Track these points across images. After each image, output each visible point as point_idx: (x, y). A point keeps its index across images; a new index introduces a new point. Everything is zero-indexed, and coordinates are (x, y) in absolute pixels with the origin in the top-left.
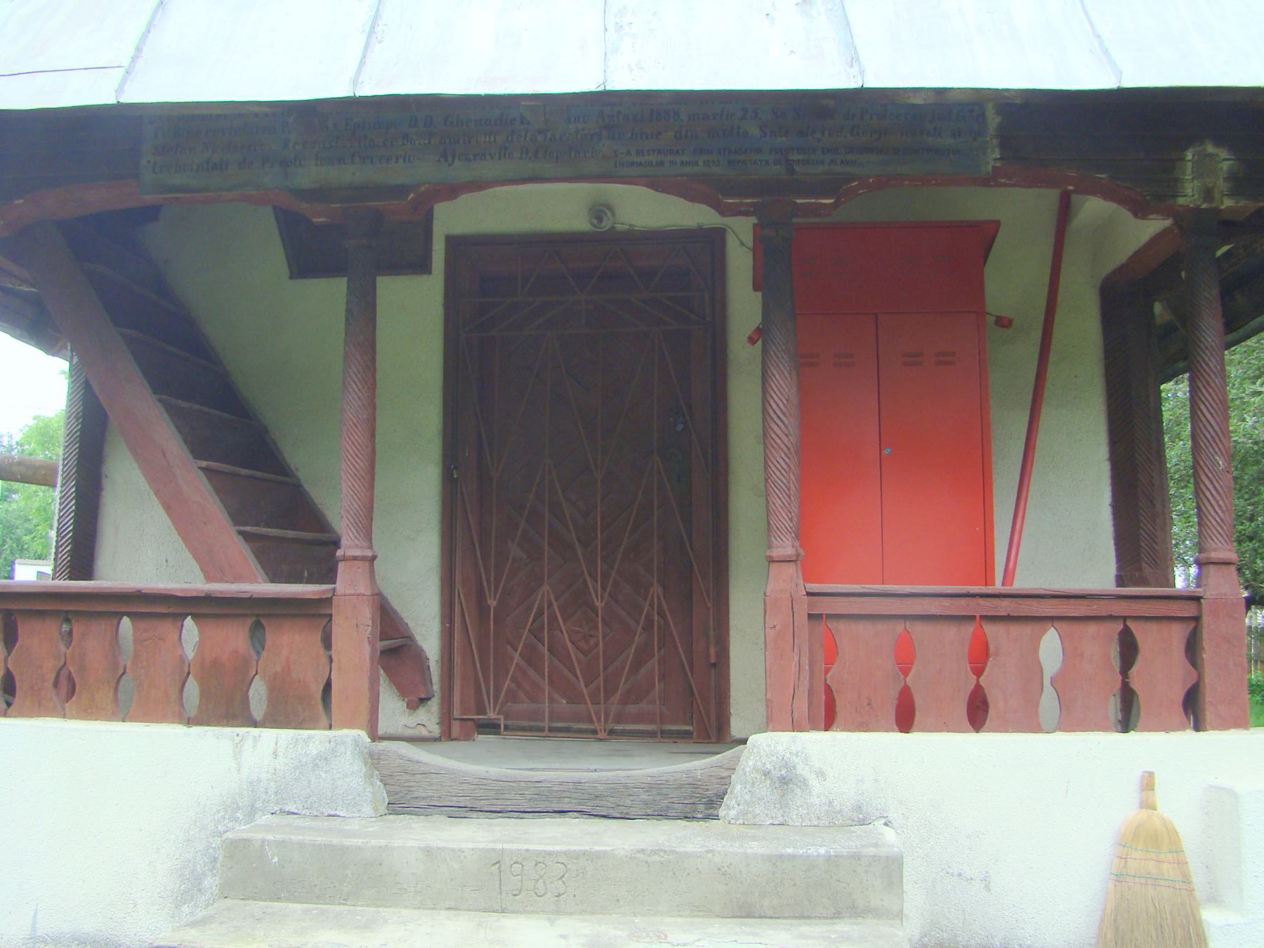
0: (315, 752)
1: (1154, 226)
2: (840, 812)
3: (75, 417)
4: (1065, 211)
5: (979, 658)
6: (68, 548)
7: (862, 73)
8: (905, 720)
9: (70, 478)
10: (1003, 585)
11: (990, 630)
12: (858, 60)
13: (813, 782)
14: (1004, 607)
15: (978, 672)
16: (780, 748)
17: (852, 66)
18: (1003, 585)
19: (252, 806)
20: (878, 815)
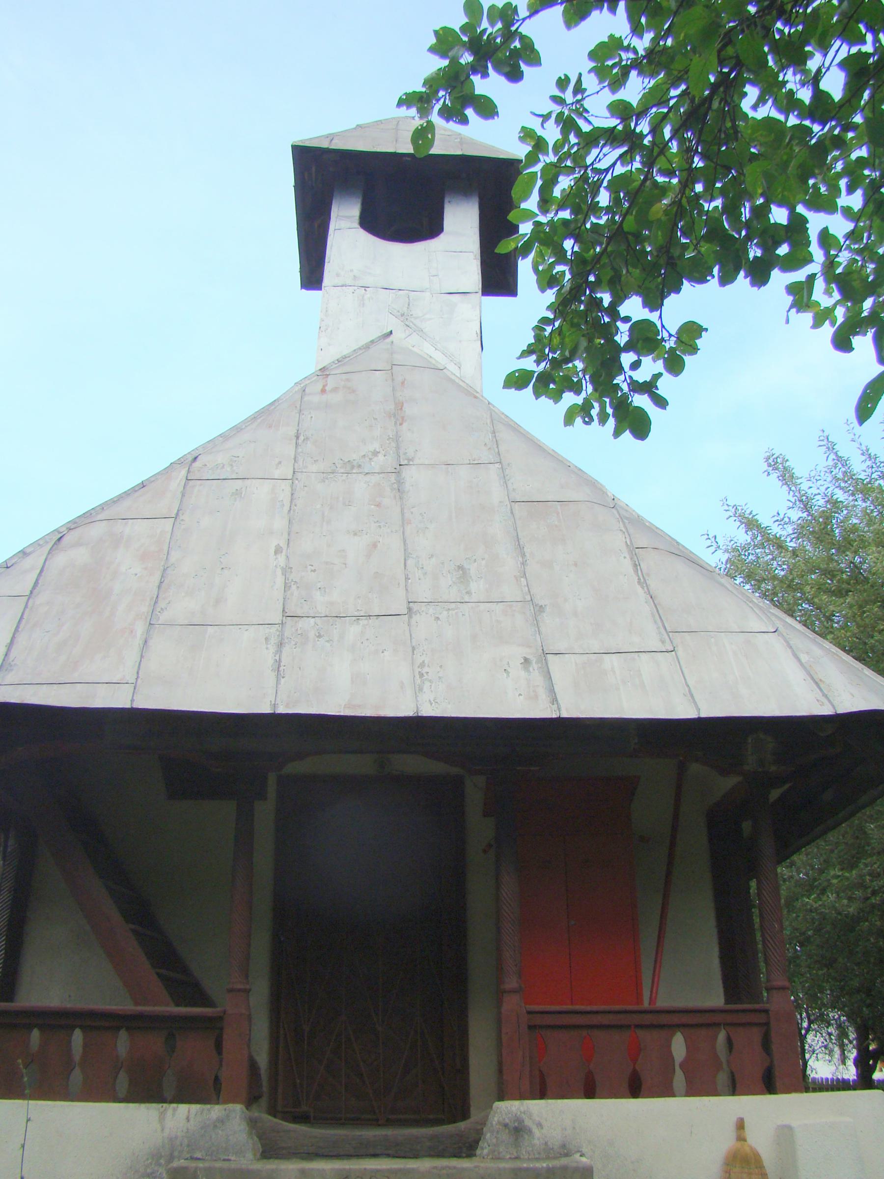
3: (7, 890)
5: (635, 1051)
7: (559, 709)
8: (590, 1092)
11: (640, 1033)
13: (536, 1130)
14: (648, 1019)
15: (634, 1060)
16: (514, 1109)
18: (650, 1004)
20: (576, 1150)
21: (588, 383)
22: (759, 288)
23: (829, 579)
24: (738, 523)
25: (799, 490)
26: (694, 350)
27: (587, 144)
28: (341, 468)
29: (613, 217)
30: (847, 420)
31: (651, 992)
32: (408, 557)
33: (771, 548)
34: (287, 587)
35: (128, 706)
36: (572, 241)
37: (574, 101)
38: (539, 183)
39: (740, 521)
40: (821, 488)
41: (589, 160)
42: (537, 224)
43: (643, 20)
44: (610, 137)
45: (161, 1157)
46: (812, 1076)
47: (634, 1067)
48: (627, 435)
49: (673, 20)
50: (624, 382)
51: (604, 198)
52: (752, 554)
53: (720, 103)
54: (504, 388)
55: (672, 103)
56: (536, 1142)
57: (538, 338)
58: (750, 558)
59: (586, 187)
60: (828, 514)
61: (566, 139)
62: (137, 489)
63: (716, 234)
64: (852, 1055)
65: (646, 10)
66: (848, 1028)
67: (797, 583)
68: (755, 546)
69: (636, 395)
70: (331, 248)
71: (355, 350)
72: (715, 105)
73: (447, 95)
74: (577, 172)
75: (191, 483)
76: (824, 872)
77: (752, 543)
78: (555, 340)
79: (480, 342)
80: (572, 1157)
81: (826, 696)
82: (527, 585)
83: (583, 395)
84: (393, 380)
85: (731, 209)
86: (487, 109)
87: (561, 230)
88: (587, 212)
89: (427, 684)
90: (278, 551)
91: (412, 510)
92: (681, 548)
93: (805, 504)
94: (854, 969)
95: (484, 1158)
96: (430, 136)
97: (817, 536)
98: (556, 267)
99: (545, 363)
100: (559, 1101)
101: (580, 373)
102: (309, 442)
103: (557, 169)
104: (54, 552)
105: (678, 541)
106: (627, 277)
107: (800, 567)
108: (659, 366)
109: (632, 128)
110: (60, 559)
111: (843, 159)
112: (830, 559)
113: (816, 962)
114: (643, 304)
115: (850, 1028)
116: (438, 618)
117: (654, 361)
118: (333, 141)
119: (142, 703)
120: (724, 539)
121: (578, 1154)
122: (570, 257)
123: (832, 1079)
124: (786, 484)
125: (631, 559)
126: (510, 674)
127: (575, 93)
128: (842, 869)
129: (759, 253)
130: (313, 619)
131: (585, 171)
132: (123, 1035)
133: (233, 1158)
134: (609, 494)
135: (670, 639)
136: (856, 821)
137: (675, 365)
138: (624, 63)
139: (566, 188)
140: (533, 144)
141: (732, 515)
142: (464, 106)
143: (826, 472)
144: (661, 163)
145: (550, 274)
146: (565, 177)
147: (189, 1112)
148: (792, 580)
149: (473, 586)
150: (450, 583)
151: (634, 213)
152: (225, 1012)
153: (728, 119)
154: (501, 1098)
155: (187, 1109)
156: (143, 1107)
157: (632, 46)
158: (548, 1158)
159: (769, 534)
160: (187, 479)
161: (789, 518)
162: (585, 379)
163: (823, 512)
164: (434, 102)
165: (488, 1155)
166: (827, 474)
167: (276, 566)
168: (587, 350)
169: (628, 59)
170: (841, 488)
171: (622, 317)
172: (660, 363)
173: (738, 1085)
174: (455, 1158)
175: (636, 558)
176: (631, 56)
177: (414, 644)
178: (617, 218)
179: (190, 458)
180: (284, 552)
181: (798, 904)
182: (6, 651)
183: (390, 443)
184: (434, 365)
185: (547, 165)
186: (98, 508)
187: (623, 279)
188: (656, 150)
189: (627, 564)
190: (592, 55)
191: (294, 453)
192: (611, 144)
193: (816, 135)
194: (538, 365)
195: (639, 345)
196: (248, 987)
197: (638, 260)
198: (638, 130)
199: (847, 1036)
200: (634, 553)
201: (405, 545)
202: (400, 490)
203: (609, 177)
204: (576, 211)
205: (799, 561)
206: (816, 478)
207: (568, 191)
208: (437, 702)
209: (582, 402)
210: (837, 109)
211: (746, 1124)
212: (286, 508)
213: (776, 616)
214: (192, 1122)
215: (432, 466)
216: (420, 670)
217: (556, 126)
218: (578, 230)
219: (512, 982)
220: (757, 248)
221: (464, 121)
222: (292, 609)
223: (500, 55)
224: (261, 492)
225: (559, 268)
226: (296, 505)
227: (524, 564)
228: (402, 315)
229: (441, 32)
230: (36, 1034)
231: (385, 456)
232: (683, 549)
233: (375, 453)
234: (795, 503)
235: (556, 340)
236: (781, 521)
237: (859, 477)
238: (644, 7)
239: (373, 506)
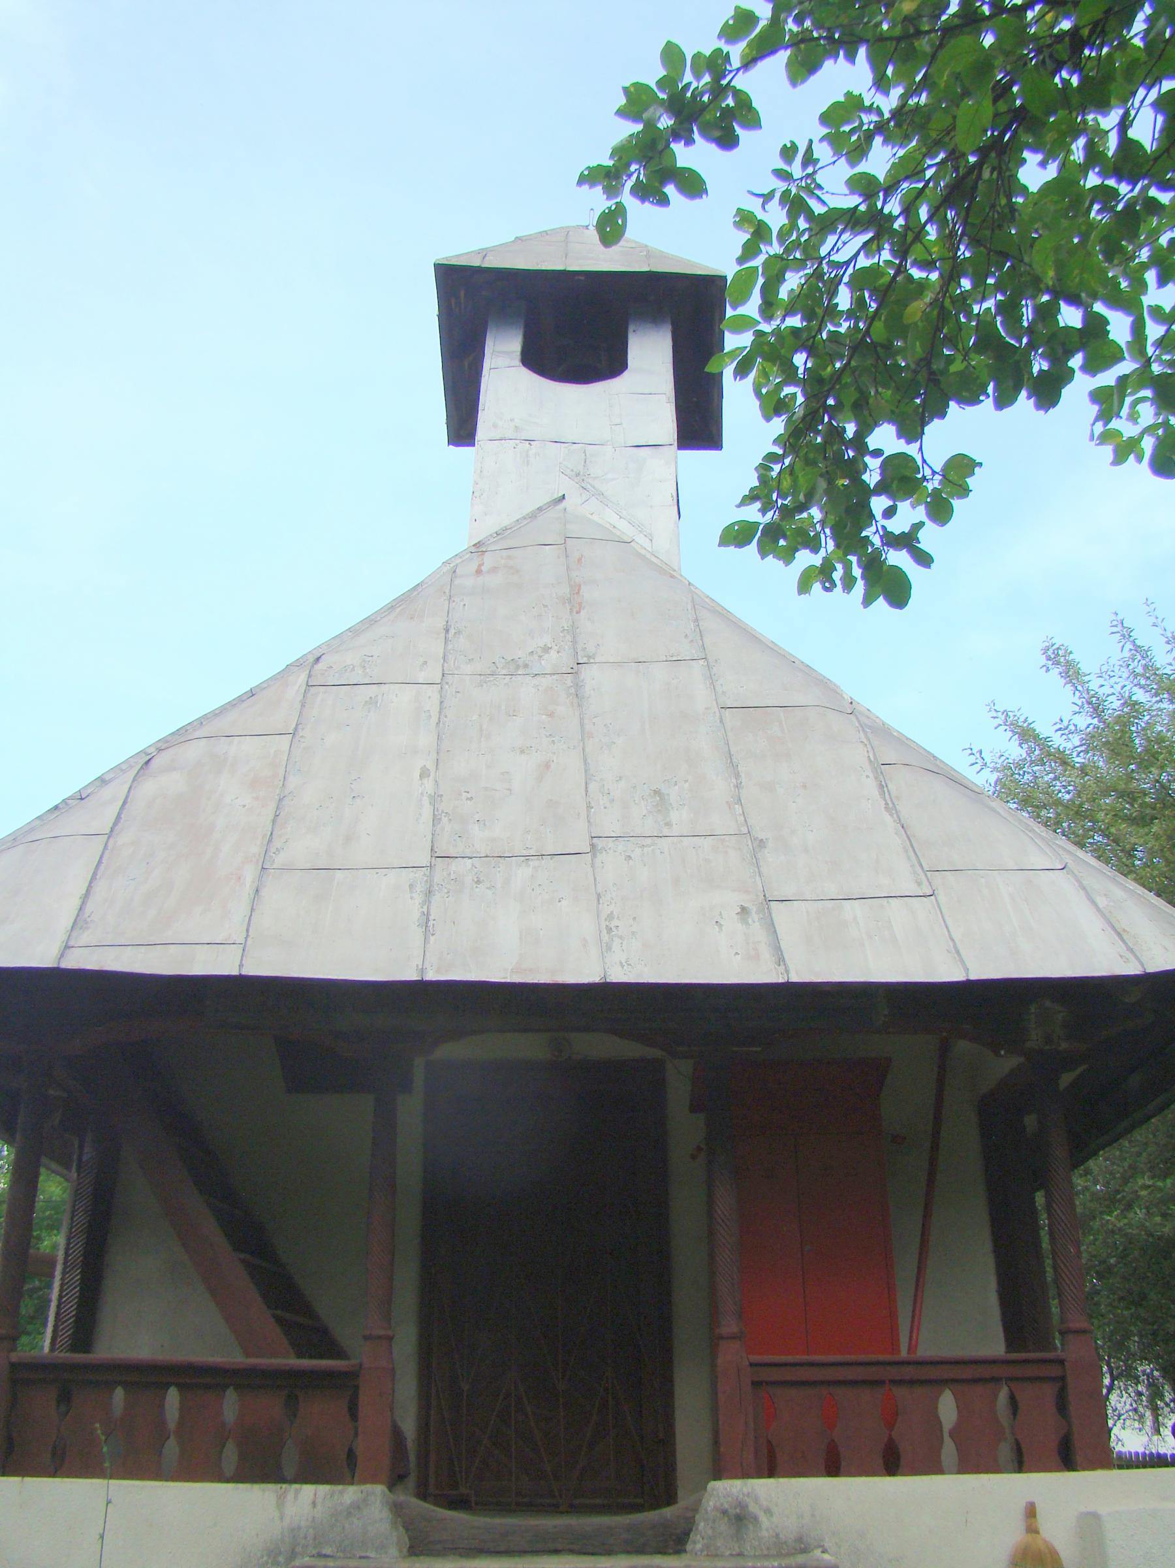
0: (349, 1502)
1: (1014, 1061)
2: (785, 1543)
4: (944, 1049)
5: (891, 1417)
6: (69, 1333)
7: (787, 971)
8: (833, 1468)
9: (74, 1267)
10: (908, 1353)
11: (900, 1392)
12: (784, 960)
13: (763, 1518)
14: (908, 1372)
15: (890, 1425)
16: (734, 1490)
17: (779, 965)
19: (293, 1550)
21: (828, 538)
22: (1046, 412)
23: (1128, 803)
24: (1010, 734)
25: (1088, 690)
26: (964, 491)
27: (822, 229)
28: (503, 668)
29: (856, 324)
30: (1147, 599)
31: (911, 1337)
32: (590, 779)
33: (1053, 764)
34: (436, 820)
35: (235, 972)
36: (804, 356)
37: (804, 175)
38: (761, 281)
39: (1012, 731)
40: (1115, 686)
41: (823, 251)
42: (759, 334)
43: (890, 71)
44: (851, 220)
45: (280, 1553)
46: (1117, 1449)
47: (890, 1435)
48: (881, 602)
49: (926, 71)
50: (875, 533)
51: (844, 299)
52: (1028, 773)
53: (992, 173)
54: (720, 545)
55: (929, 174)
56: (765, 1533)
57: (764, 480)
58: (1025, 777)
59: (820, 285)
60: (1125, 720)
61: (793, 225)
62: (244, 698)
63: (988, 340)
64: (1169, 1422)
65: (895, 54)
66: (1163, 1387)
67: (1088, 810)
68: (1032, 762)
69: (891, 550)
70: (486, 391)
71: (518, 520)
72: (986, 174)
73: (642, 168)
74: (808, 267)
75: (312, 689)
76: (1129, 1182)
77: (1028, 759)
78: (785, 483)
79: (676, 507)
80: (811, 1554)
81: (1131, 950)
82: (743, 813)
83: (822, 553)
84: (567, 556)
85: (1009, 310)
86: (693, 185)
87: (790, 341)
88: (823, 317)
89: (617, 941)
90: (424, 773)
91: (594, 720)
92: (938, 763)
93: (1097, 708)
94: (1170, 1308)
95: (696, 1554)
96: (620, 222)
97: (1112, 748)
98: (784, 388)
99: (772, 512)
100: (793, 1480)
101: (818, 526)
102: (461, 636)
103: (785, 262)
104: (140, 779)
105: (935, 755)
106: (876, 398)
107: (1090, 788)
108: (920, 514)
109: (879, 207)
110: (148, 788)
111: (1147, 245)
112: (1130, 777)
113: (1122, 1298)
114: (897, 436)
115: (1166, 1387)
116: (630, 857)
117: (913, 507)
118: (487, 258)
119: (251, 970)
120: (992, 754)
121: (820, 1550)
122: (802, 376)
123: (1144, 1454)
124: (1070, 682)
125: (876, 778)
126: (723, 928)
127: (805, 165)
128: (1153, 1177)
129: (1045, 366)
130: (470, 860)
131: (820, 264)
132: (231, 1396)
133: (372, 1555)
134: (846, 697)
135: (928, 879)
136: (1170, 1116)
137: (940, 511)
138: (865, 127)
139: (795, 288)
140: (752, 230)
141: (1001, 723)
142: (663, 183)
143: (1121, 666)
144: (917, 252)
145: (776, 399)
146: (793, 274)
147: (315, 1495)
148: (1081, 806)
149: (674, 816)
150: (645, 812)
151: (883, 318)
152: (361, 1365)
153: (1002, 196)
154: (718, 1476)
155: (313, 1492)
156: (257, 1488)
157: (875, 106)
158: (779, 1555)
159: (1049, 747)
160: (307, 685)
161: (1075, 726)
162: (825, 533)
163: (1119, 716)
164: (625, 178)
165: (702, 1551)
166: (1122, 669)
167: (422, 794)
168: (827, 492)
169: (870, 123)
170: (1141, 687)
171: (871, 450)
172: (921, 509)
173: (1025, 1459)
174: (659, 1556)
175: (881, 777)
176: (874, 118)
177: (599, 890)
178: (861, 325)
179: (311, 659)
180: (432, 775)
181: (1096, 1224)
182: (80, 903)
183: (565, 636)
184: (619, 537)
185: (771, 257)
186: (195, 723)
187: (871, 401)
188: (910, 237)
189: (870, 786)
190: (825, 119)
191: (442, 651)
192: (852, 229)
193: (1123, 198)
194: (764, 514)
195: (894, 486)
196: (390, 1333)
197: (891, 377)
198: (886, 211)
199: (1162, 1398)
200: (879, 771)
201: (585, 764)
202: (578, 695)
203: (850, 271)
204: (809, 316)
205: (1089, 780)
206: (1109, 673)
207: (797, 292)
208: (630, 965)
209: (821, 562)
210: (1151, 163)
211: (1038, 1510)
212: (435, 719)
213: (1065, 850)
214: (319, 1507)
215: (619, 664)
216: (608, 924)
217: (780, 208)
218: (812, 340)
219: (730, 1325)
220: (1043, 360)
221: (664, 201)
222: (443, 848)
223: (708, 116)
224: (401, 699)
225: (788, 390)
226: (446, 717)
227: (738, 786)
228: (578, 475)
229: (632, 90)
230: (119, 1393)
231: (558, 652)
232: (942, 766)
233: (546, 649)
234: (1082, 707)
235: (786, 483)
236: (1064, 730)
237: (1164, 672)
238: (892, 50)
239: (544, 716)
